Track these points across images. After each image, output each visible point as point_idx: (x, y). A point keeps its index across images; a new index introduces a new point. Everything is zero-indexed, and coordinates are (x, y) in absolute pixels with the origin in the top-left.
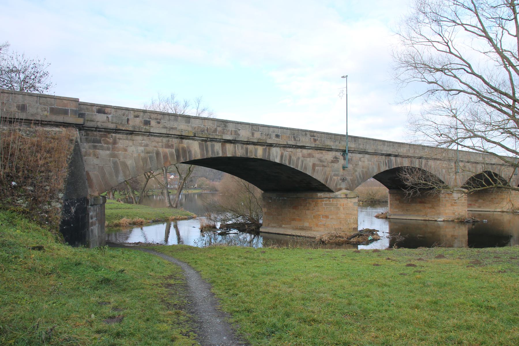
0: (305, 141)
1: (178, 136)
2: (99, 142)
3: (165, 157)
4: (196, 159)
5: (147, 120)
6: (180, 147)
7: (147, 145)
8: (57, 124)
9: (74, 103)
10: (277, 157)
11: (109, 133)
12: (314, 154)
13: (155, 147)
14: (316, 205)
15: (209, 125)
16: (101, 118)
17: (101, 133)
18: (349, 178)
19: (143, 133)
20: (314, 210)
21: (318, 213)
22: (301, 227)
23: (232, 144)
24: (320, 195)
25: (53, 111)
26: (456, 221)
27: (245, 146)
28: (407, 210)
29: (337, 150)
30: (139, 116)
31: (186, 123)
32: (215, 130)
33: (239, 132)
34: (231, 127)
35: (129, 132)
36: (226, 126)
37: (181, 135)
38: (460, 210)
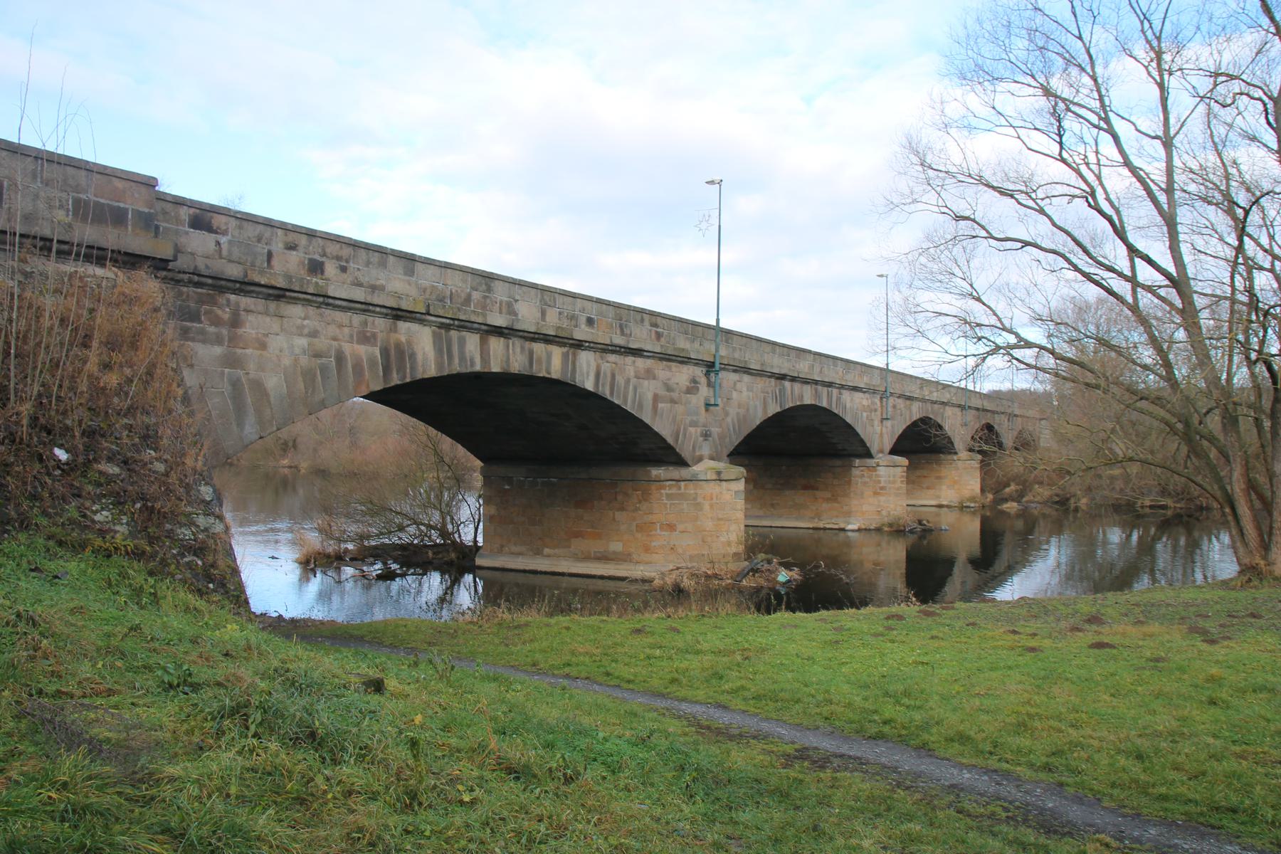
0: (641, 337)
1: (389, 311)
2: (195, 317)
3: (358, 368)
4: (426, 376)
5: (315, 260)
6: (392, 341)
7: (314, 334)
8: (96, 255)
9: (143, 189)
10: (588, 375)
11: (222, 290)
12: (656, 372)
13: (335, 339)
14: (646, 496)
15: (455, 283)
16: (199, 243)
17: (199, 290)
18: (715, 430)
19: (309, 297)
20: (637, 509)
21: (650, 518)
22: (598, 555)
23: (502, 339)
24: (656, 472)
25: (81, 210)
26: (886, 529)
27: (527, 344)
28: (772, 505)
29: (698, 363)
30: (296, 246)
31: (405, 274)
32: (468, 300)
33: (518, 306)
34: (501, 294)
35: (276, 292)
36: (489, 289)
37: (399, 309)
38: (892, 506)
